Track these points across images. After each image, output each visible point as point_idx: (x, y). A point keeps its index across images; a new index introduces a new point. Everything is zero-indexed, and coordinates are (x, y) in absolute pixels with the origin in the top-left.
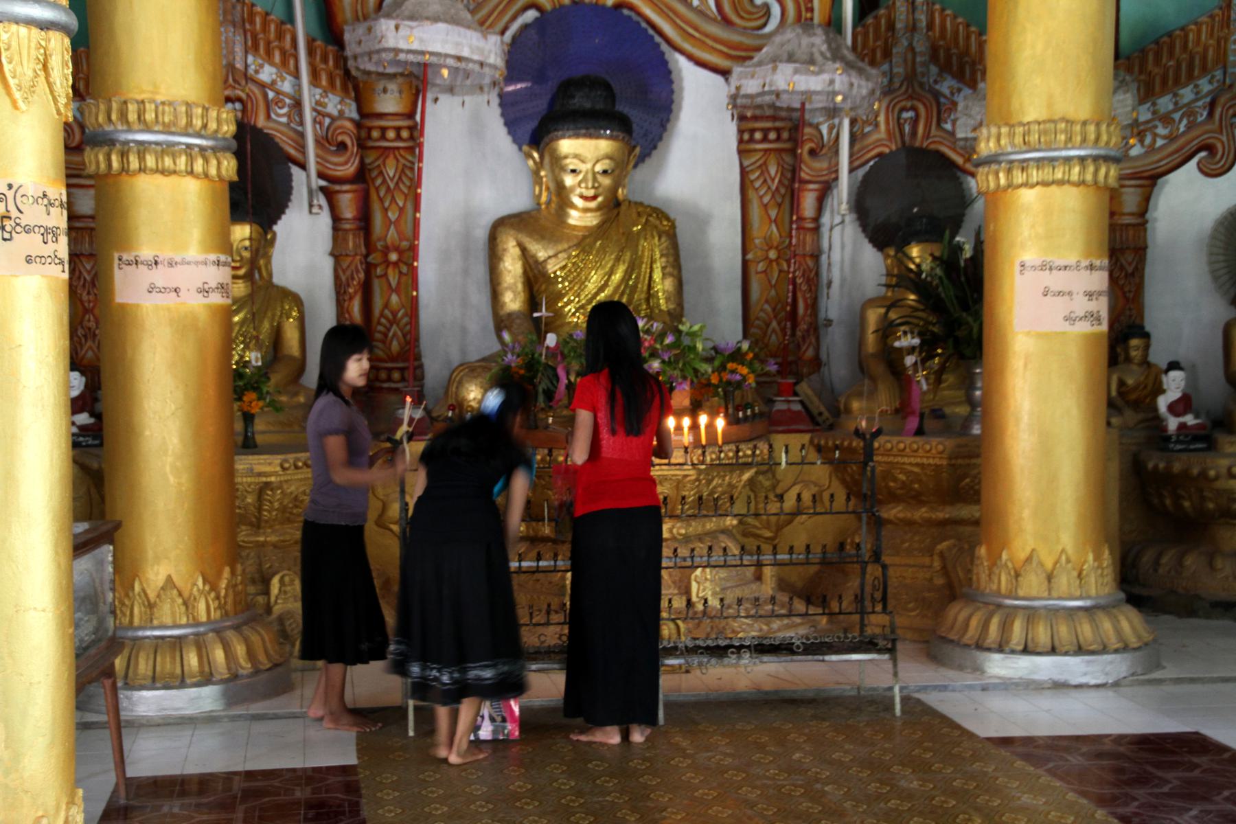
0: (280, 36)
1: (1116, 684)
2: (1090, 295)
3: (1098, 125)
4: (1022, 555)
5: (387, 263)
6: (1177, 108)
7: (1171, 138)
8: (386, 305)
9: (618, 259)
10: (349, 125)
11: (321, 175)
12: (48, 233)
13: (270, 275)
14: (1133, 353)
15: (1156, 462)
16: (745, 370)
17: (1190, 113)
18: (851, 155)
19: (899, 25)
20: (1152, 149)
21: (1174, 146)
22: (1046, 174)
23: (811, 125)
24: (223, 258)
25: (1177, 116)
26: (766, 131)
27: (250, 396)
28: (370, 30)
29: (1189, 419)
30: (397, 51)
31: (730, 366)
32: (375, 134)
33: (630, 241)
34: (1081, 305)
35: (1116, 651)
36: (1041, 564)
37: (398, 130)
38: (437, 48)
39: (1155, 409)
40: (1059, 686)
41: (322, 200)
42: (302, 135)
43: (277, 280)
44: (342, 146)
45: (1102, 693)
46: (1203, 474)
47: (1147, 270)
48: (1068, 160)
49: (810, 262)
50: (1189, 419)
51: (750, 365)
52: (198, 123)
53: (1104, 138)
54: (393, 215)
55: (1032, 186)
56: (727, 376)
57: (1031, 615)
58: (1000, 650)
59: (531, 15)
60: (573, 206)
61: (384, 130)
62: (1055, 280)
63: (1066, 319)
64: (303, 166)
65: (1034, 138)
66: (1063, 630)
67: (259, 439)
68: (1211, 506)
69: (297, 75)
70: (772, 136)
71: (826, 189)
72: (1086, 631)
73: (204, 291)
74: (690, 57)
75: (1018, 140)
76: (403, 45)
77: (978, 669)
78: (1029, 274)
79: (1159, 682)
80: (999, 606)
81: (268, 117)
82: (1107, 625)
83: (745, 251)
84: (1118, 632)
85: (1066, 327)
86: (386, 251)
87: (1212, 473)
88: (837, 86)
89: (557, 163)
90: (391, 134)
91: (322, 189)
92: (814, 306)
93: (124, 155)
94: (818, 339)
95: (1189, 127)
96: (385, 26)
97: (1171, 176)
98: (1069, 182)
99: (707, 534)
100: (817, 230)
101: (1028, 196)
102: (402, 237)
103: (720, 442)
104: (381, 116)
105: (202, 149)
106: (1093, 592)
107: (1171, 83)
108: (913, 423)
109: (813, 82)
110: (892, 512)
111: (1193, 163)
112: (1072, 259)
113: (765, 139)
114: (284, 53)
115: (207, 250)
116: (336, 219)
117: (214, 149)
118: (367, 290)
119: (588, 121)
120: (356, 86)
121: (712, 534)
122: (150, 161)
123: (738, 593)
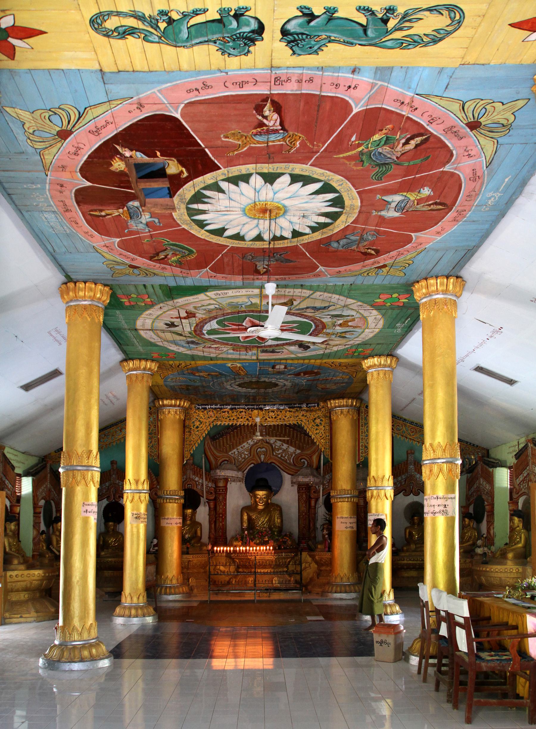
0: (200, 472)
3: (351, 490)
5: (219, 517)
6: (397, 481)
8: (219, 525)
11: (206, 499)
12: (145, 518)
18: (323, 493)
27: (188, 544)
30: (220, 476)
34: (348, 525)
37: (223, 490)
41: (207, 504)
42: (203, 491)
43: (197, 520)
44: (211, 493)
54: (221, 507)
57: (337, 586)
59: (252, 465)
62: (343, 520)
64: (203, 497)
66: (343, 589)
67: (190, 552)
69: (203, 479)
71: (317, 500)
73: (176, 524)
74: (287, 473)
86: (219, 514)
89: (255, 496)
92: (314, 525)
93: (163, 500)
95: (401, 486)
96: (218, 471)
103: (205, 538)
104: (220, 487)
108: (327, 549)
110: (323, 568)
113: (302, 490)
116: (210, 508)
118: (215, 522)
122: (168, 501)
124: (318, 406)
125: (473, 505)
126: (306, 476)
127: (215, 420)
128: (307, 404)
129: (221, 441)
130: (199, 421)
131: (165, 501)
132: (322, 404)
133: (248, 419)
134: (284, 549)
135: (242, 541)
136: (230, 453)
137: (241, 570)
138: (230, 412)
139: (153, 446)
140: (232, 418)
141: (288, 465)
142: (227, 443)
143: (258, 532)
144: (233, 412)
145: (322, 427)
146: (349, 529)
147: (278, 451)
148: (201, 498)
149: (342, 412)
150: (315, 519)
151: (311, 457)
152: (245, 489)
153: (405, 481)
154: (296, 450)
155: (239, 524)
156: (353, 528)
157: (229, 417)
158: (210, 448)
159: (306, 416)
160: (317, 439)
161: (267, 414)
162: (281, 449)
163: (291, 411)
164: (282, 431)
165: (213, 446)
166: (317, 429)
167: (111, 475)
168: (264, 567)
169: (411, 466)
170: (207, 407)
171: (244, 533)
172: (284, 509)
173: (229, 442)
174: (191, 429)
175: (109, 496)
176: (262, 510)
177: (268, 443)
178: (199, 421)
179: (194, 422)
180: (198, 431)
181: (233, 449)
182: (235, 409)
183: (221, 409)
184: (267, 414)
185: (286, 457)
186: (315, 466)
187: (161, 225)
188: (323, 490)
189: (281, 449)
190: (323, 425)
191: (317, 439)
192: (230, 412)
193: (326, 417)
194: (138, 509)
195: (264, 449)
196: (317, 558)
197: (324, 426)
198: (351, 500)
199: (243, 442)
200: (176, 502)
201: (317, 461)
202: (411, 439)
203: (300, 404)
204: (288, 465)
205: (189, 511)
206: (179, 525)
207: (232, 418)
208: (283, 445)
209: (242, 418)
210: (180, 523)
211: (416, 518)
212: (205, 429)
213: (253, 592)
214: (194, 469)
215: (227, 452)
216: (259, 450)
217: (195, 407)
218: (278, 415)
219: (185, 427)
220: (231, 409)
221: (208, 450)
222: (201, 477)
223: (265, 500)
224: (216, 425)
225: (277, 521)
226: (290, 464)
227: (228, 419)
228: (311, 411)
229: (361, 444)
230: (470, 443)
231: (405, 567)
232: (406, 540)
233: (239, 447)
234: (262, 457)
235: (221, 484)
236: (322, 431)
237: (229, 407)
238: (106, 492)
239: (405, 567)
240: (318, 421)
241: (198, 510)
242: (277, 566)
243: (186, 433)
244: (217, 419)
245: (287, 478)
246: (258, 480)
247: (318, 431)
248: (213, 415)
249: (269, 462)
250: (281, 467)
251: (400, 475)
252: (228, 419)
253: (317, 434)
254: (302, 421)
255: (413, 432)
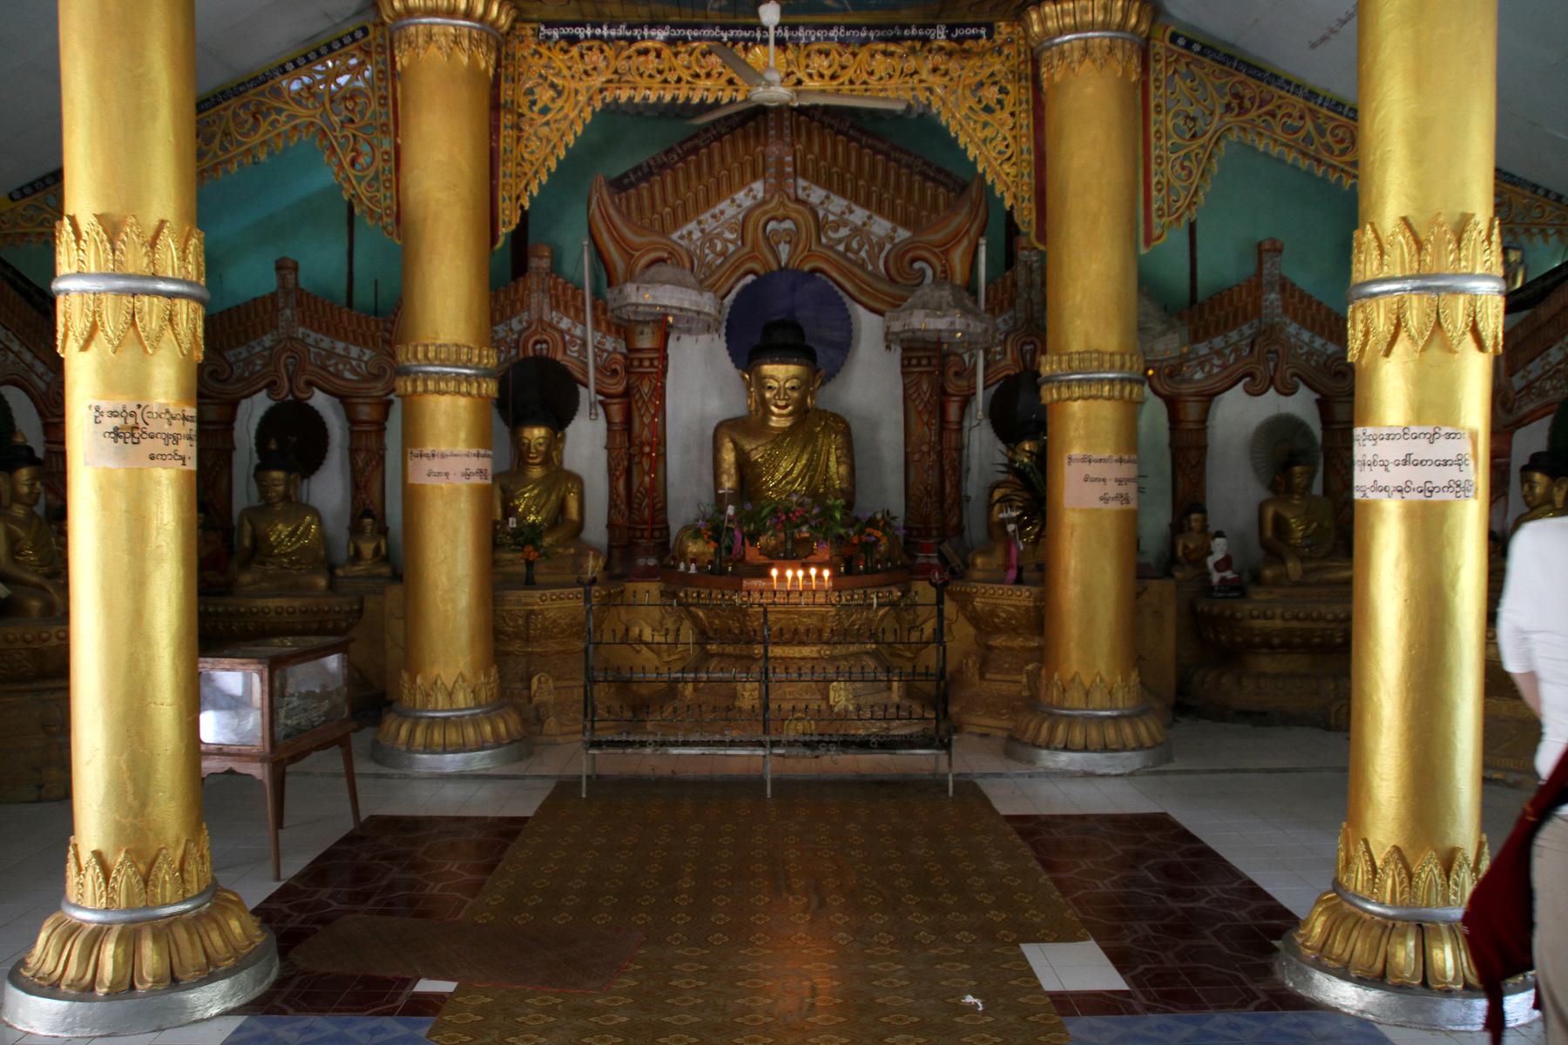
0: (574, 298)
1: (1132, 774)
2: (1119, 481)
3: (1122, 355)
4: (1069, 677)
5: (642, 454)
6: (1227, 346)
7: (1224, 367)
9: (802, 452)
10: (619, 357)
11: (598, 392)
13: (561, 462)
14: (1194, 524)
15: (1203, 606)
16: (879, 534)
17: (1236, 350)
19: (1021, 283)
20: (1209, 376)
21: (1226, 373)
22: (1086, 391)
23: (956, 354)
24: (482, 451)
25: (1228, 351)
26: (919, 359)
27: (529, 548)
28: (621, 291)
29: (1229, 575)
30: (637, 305)
31: (868, 530)
32: (636, 363)
33: (810, 439)
34: (1112, 489)
35: (1133, 749)
36: (1082, 684)
37: (651, 360)
38: (666, 302)
39: (1205, 565)
40: (1088, 775)
41: (600, 410)
42: (586, 364)
43: (567, 465)
44: (615, 372)
45: (1120, 781)
46: (1232, 616)
47: (1208, 463)
48: (1101, 380)
49: (955, 454)
50: (1229, 575)
51: (883, 530)
52: (464, 357)
53: (1128, 364)
54: (646, 420)
55: (1076, 399)
56: (864, 538)
57: (1071, 721)
58: (1047, 747)
59: (750, 278)
60: (773, 414)
61: (641, 360)
62: (1093, 470)
63: (1102, 499)
64: (586, 386)
65: (1075, 364)
66: (1094, 734)
67: (539, 579)
68: (1239, 639)
69: (584, 324)
70: (924, 362)
71: (966, 401)
72: (1111, 734)
73: (467, 475)
74: (866, 306)
75: (1064, 365)
76: (641, 301)
77: (1031, 761)
78: (1074, 465)
79: (1165, 772)
80: (1051, 714)
81: (565, 352)
82: (1127, 730)
83: (906, 445)
84: (1137, 736)
85: (1101, 505)
87: (1239, 615)
88: (957, 326)
89: (761, 383)
90: (647, 363)
91: (601, 403)
92: (958, 485)
93: (415, 381)
94: (961, 511)
95: (1237, 360)
96: (630, 288)
97: (1227, 395)
98: (1102, 397)
99: (852, 655)
100: (960, 430)
101: (1076, 407)
102: (653, 434)
104: (640, 350)
105: (467, 376)
106: (1120, 704)
107: (1223, 327)
108: (1012, 574)
109: (940, 324)
110: (998, 641)
111: (1240, 385)
112: (1106, 454)
113: (919, 364)
114: (576, 309)
115: (470, 446)
116: (609, 423)
117: (476, 376)
119: (782, 353)
120: (624, 328)
121: (856, 655)
122: (431, 385)
123: (871, 699)
124: (990, 36)
125: (1546, 422)
126: (936, 309)
127: (610, 81)
128: (951, 28)
129: (645, 194)
130: (553, 86)
131: (420, 389)
132: (1003, 28)
133: (731, 82)
134: (866, 572)
135: (717, 541)
136: (675, 236)
137: (713, 648)
138: (666, 53)
139: (376, 177)
140: (672, 77)
141: (870, 280)
142: (665, 201)
143: (775, 511)
144: (676, 55)
145: (1005, 115)
146: (1114, 506)
147: (836, 230)
148: (582, 389)
149: (1086, 51)
150: (959, 470)
151: (946, 253)
152: (729, 359)
153: (1252, 345)
154: (894, 230)
155: (708, 478)
156: (1127, 501)
157: (660, 72)
158: (607, 218)
159: (946, 73)
160: (987, 160)
161: (803, 62)
162: (845, 224)
163: (892, 54)
164: (849, 164)
165: (618, 210)
166: (985, 125)
167: (276, 309)
168: (797, 638)
169: (1273, 296)
170: (580, 32)
171: (723, 511)
172: (855, 429)
173: (670, 199)
174: (521, 115)
175: (274, 383)
176: (785, 433)
177: (804, 203)
178: (553, 86)
179: (530, 92)
180: (547, 123)
181: (686, 220)
182: (685, 40)
183: (632, 40)
184: (803, 62)
185: (863, 254)
186: (958, 280)
187: (774, 572)
188: (986, 368)
189: (845, 224)
190: (1009, 108)
191: (987, 160)
192: (666, 53)
193: (1018, 77)
194: (140, 385)
195: (788, 224)
196: (978, 603)
197: (1012, 114)
198: (1122, 389)
199: (720, 198)
200: (464, 389)
201: (967, 266)
202: (1334, 167)
203: (924, 27)
204: (870, 280)
205: (537, 434)
206: (476, 480)
207: (672, 77)
208: (851, 212)
209: (708, 75)
210: (481, 472)
211: (1297, 469)
212: (572, 115)
213: (760, 752)
214: (555, 288)
215: (664, 232)
216: (772, 225)
217: (537, 32)
218: (843, 68)
219: (496, 107)
220: (670, 41)
221: (601, 225)
222: (579, 316)
223: (795, 395)
224: (616, 100)
225: (836, 470)
226: (875, 275)
227: (659, 78)
228: (967, 54)
229: (1154, 180)
230: (1547, 192)
231: (1276, 641)
232: (1264, 544)
233: (706, 216)
234: (784, 250)
235: (646, 341)
236: (1005, 131)
237: (662, 34)
238: (264, 366)
239: (1276, 641)
240: (991, 94)
241: (570, 430)
242: (844, 635)
243: (503, 132)
244: (618, 78)
245: (868, 325)
246: (770, 328)
247: (989, 132)
248: (602, 65)
249: (807, 268)
250: (848, 286)
251: (1236, 325)
252: (659, 78)
253: (989, 145)
254: (930, 90)
255: (1342, 141)
